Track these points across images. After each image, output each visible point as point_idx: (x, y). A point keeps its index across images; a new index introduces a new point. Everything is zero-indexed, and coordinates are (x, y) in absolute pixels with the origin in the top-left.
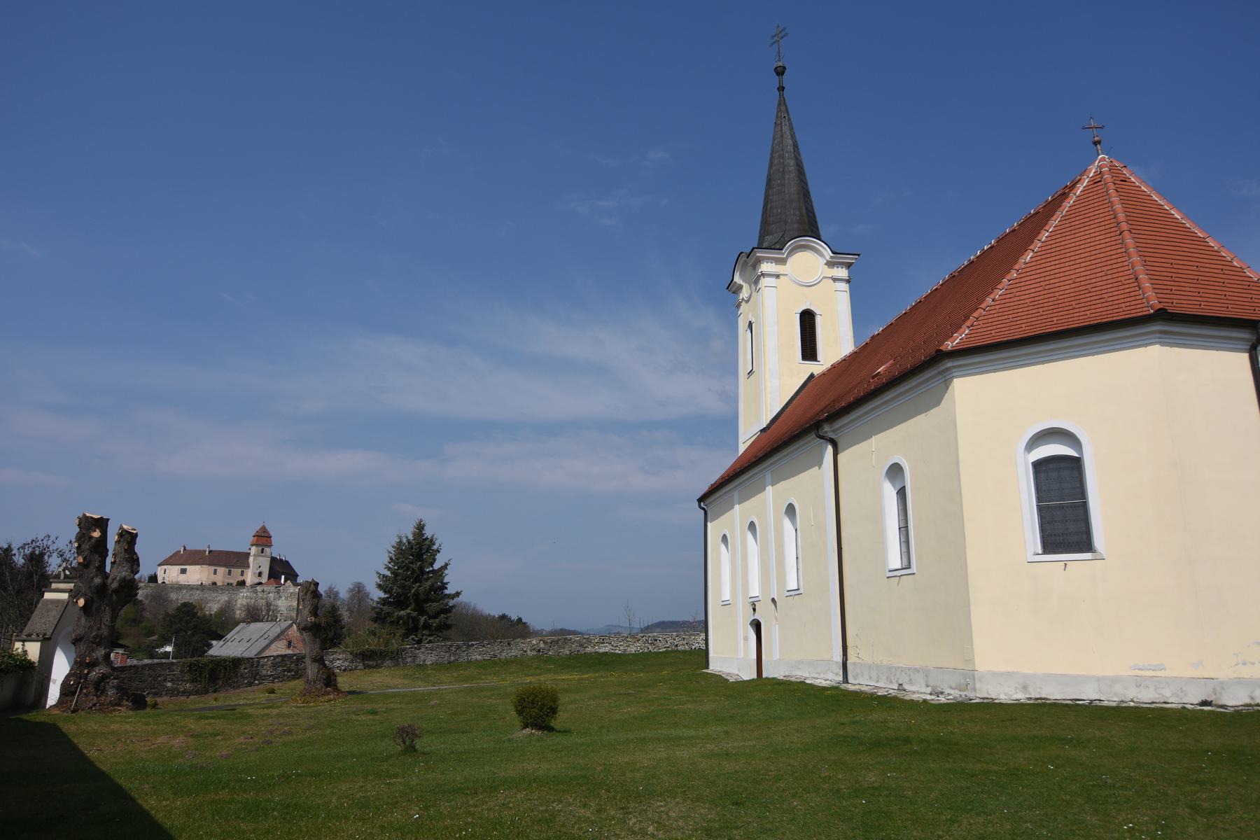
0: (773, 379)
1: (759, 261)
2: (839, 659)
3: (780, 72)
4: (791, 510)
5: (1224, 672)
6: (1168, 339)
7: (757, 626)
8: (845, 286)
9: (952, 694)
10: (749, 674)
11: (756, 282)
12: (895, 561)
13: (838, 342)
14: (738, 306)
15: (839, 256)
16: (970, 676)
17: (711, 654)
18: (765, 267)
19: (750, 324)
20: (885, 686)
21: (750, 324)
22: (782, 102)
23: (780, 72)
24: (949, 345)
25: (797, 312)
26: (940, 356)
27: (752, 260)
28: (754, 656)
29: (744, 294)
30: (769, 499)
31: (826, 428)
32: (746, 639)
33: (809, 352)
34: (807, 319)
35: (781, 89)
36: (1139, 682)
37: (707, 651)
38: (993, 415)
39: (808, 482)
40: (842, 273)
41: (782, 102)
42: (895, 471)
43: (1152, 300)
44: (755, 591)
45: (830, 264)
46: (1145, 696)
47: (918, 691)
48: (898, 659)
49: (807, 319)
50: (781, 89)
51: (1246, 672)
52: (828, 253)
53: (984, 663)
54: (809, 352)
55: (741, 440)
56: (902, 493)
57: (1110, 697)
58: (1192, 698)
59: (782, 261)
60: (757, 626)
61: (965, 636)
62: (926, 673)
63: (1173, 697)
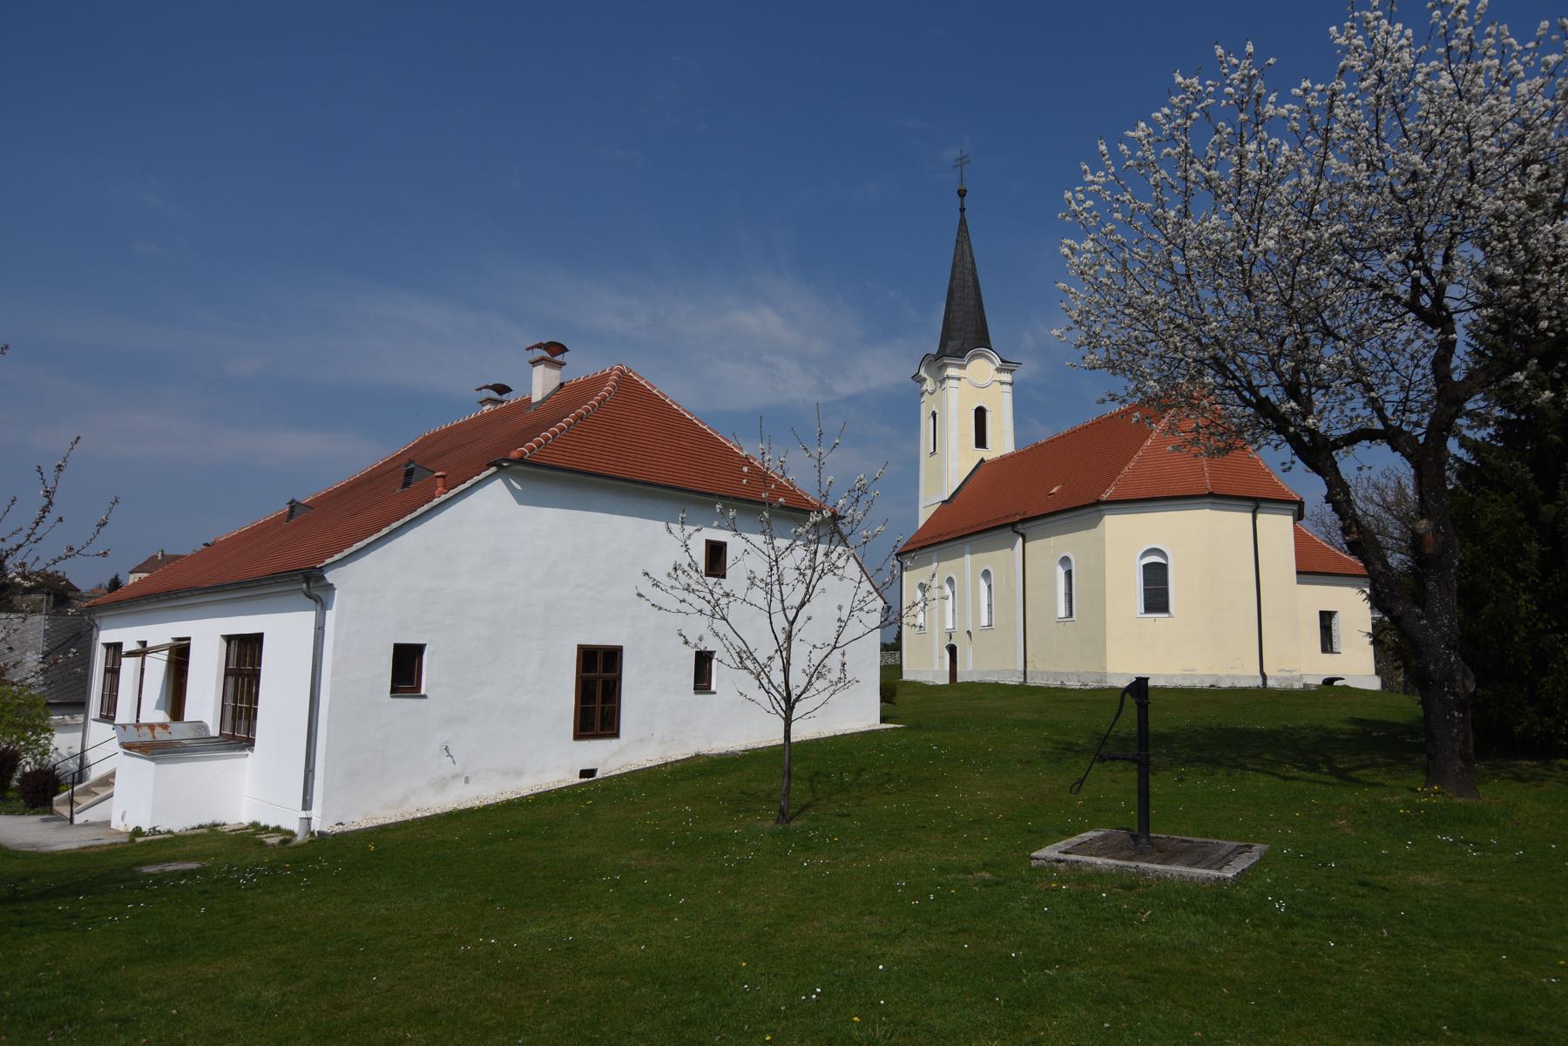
0: (949, 464)
1: (945, 366)
2: (1021, 668)
3: (962, 193)
4: (986, 574)
5: (1222, 673)
6: (1214, 507)
7: (952, 650)
8: (1008, 388)
9: (1093, 685)
10: (944, 680)
11: (942, 381)
12: (1062, 611)
13: (1002, 442)
14: (922, 394)
15: (1006, 365)
16: (1105, 674)
17: (905, 668)
18: (951, 371)
19: (934, 415)
20: (1053, 683)
21: (934, 415)
22: (963, 222)
23: (962, 193)
24: (1105, 497)
25: (971, 414)
26: (1099, 503)
27: (940, 363)
28: (947, 668)
29: (929, 385)
30: (967, 565)
31: (1019, 527)
32: (941, 657)
33: (981, 441)
34: (980, 414)
35: (962, 210)
36: (1184, 677)
37: (900, 666)
38: (1125, 537)
39: (1004, 559)
40: (1007, 377)
41: (963, 222)
42: (1065, 561)
43: (1208, 487)
44: (950, 626)
45: (999, 370)
46: (1186, 683)
47: (1073, 684)
48: (1059, 664)
49: (980, 414)
50: (962, 210)
51: (1232, 672)
52: (998, 362)
53: (1110, 669)
54: (981, 441)
55: (921, 505)
56: (1069, 574)
57: (1170, 684)
58: (1206, 684)
59: (963, 367)
60: (952, 650)
61: (1104, 654)
62: (1079, 675)
63: (1198, 683)
